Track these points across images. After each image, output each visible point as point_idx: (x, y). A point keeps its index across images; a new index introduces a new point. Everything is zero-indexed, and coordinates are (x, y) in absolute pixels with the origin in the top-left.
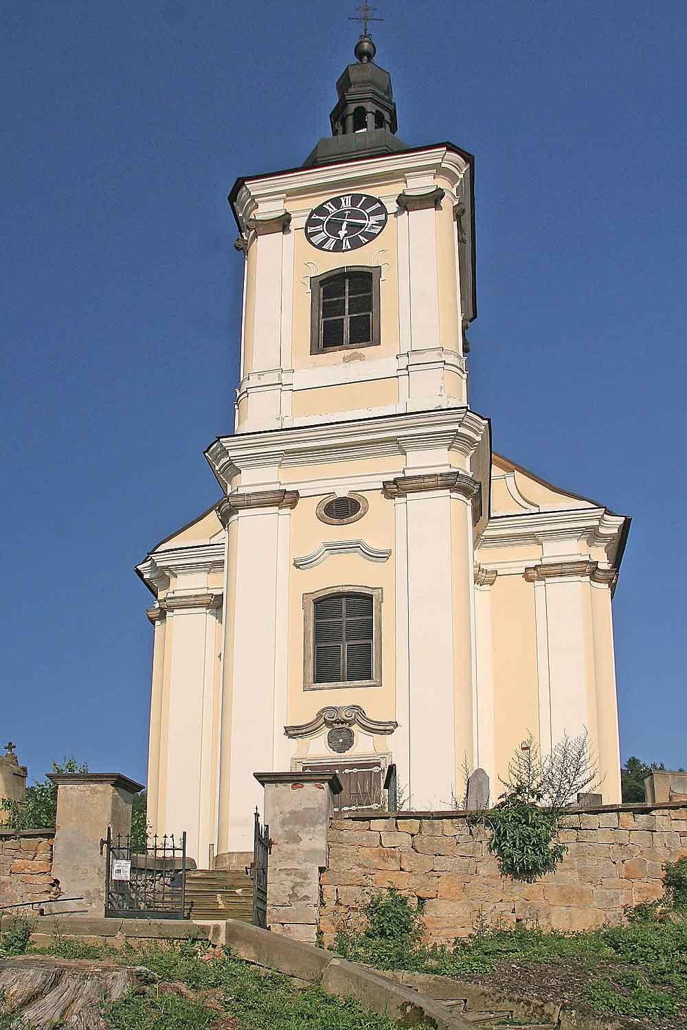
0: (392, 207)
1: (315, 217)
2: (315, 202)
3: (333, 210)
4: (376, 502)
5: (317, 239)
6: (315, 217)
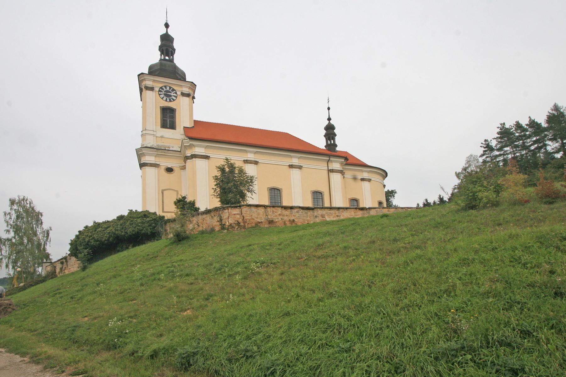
0: (179, 93)
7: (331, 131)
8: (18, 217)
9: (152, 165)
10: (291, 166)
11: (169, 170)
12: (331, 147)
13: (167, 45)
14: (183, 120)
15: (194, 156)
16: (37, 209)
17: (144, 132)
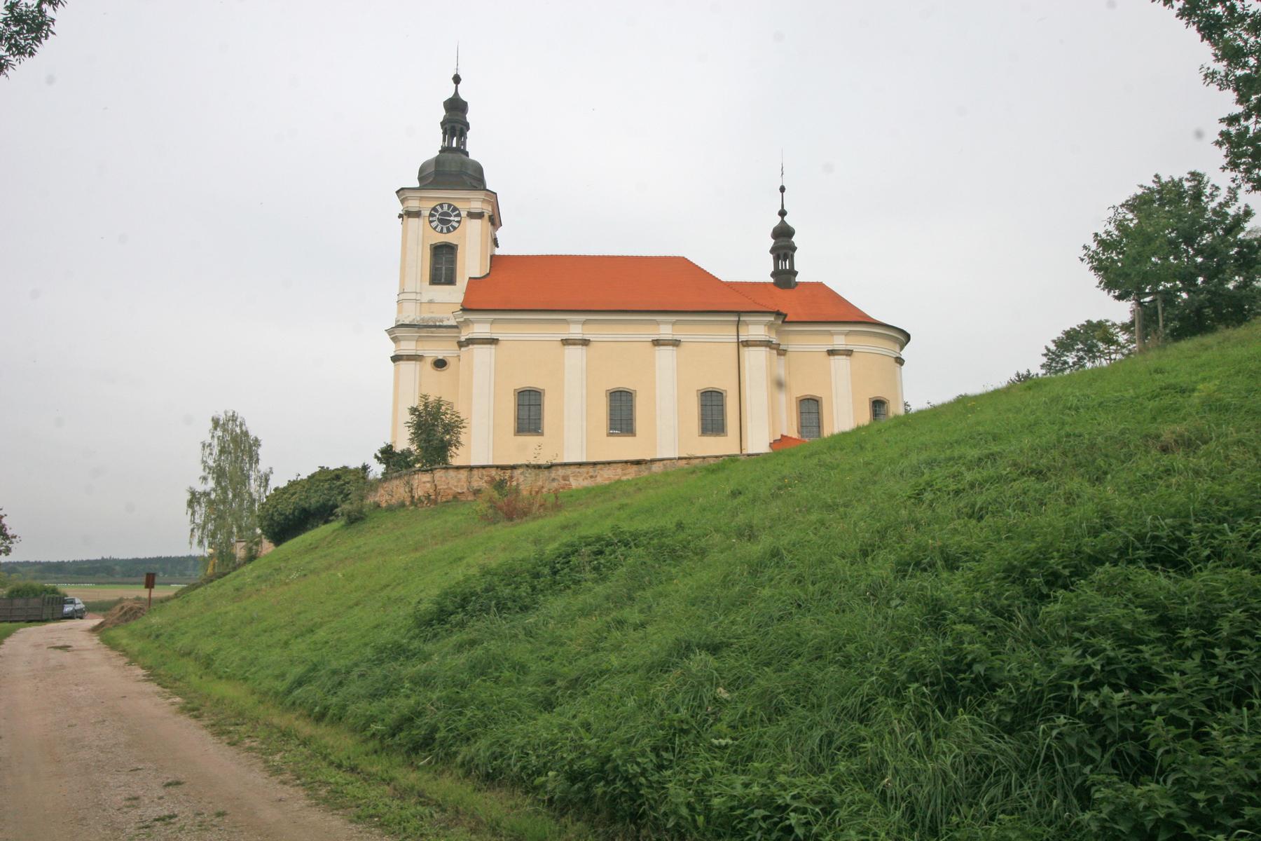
0: (464, 214)
7: (783, 242)
8: (222, 452)
9: (410, 358)
10: (657, 343)
11: (440, 364)
12: (784, 277)
13: (455, 117)
14: (471, 264)
15: (471, 341)
16: (253, 434)
17: (402, 297)
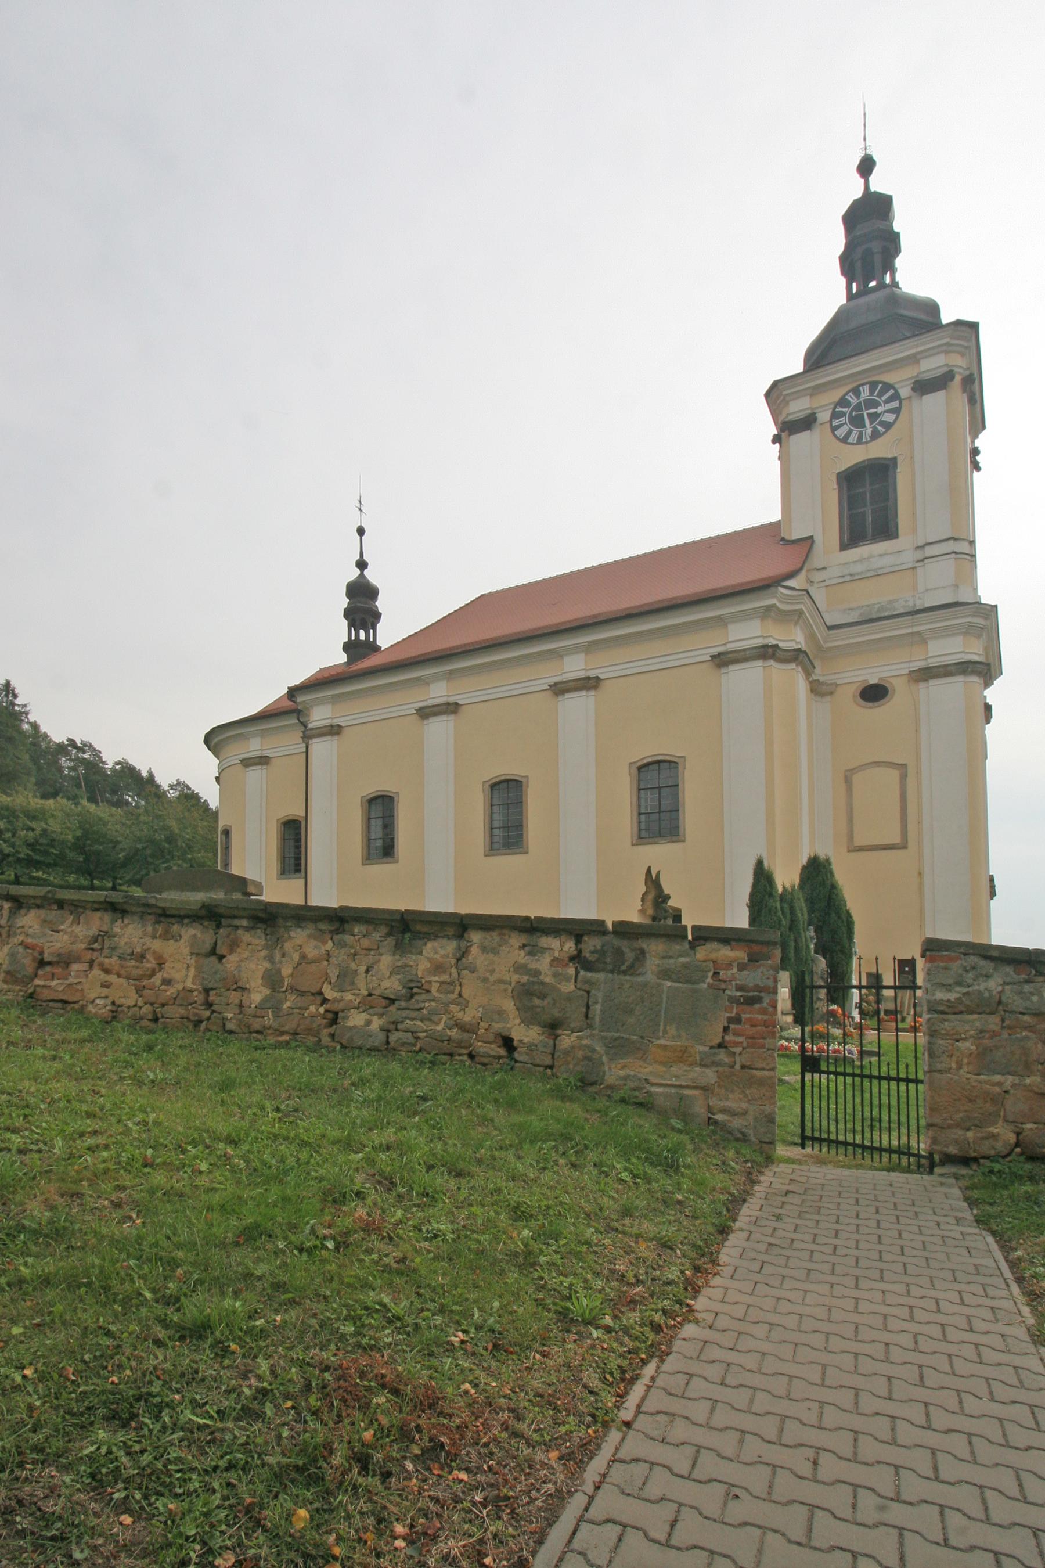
0: (905, 392)
1: (839, 409)
2: (836, 395)
3: (853, 400)
4: (900, 688)
5: (841, 432)
6: (839, 409)
13: (870, 234)
